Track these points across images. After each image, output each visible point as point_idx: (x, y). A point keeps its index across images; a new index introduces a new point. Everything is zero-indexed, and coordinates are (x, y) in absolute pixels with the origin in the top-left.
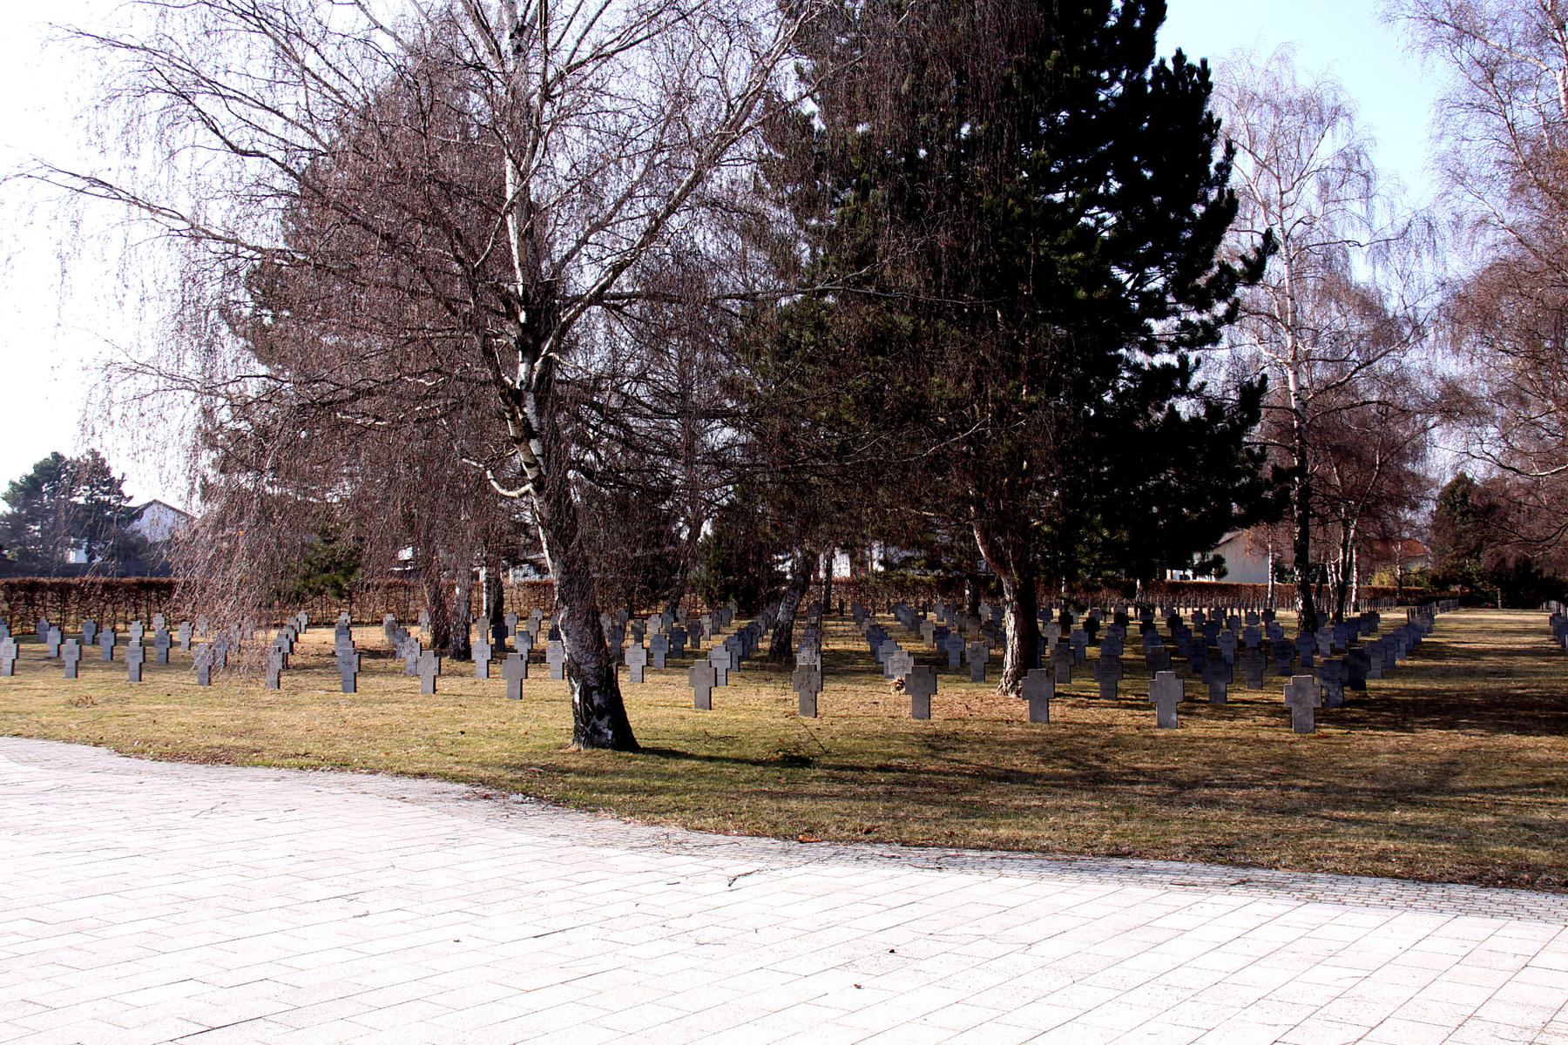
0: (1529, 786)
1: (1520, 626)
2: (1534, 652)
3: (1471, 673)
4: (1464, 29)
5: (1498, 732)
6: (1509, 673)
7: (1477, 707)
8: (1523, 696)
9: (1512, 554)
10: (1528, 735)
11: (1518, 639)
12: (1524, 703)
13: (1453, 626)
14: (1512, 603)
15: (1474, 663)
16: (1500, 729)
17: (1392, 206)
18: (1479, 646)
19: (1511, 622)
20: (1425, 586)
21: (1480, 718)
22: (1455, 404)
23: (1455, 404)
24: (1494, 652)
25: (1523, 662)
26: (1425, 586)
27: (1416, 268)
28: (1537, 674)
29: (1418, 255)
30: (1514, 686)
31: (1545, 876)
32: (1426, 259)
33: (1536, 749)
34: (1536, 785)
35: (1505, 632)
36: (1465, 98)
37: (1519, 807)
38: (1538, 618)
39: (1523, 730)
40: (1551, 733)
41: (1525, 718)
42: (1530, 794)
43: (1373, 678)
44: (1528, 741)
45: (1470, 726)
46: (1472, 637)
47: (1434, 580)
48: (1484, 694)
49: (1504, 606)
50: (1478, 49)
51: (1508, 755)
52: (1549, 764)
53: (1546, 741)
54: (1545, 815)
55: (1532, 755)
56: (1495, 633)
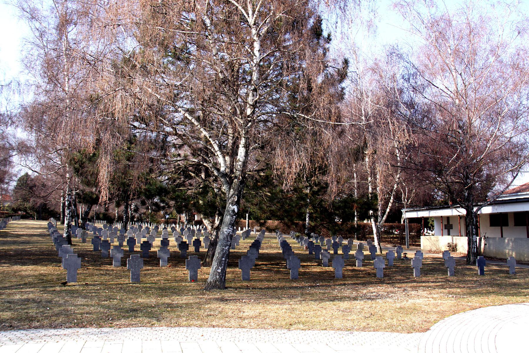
0: (17, 285)
1: (39, 226)
2: (40, 235)
3: (14, 243)
4: (33, 16)
5: (14, 265)
6: (28, 243)
7: (11, 255)
8: (29, 251)
9: (40, 201)
10: (25, 265)
11: (36, 231)
12: (29, 253)
13: (15, 225)
14: (40, 218)
15: (17, 239)
16: (16, 263)
17: (5, 74)
18: (21, 233)
19: (36, 225)
20: (10, 212)
21: (10, 260)
22: (23, 149)
23: (23, 149)
24: (26, 235)
25: (35, 238)
26: (10, 212)
27: (12, 98)
28: (38, 243)
29: (14, 93)
30: (28, 247)
31: (3, 324)
32: (17, 95)
33: (26, 271)
34: (20, 285)
35: (32, 228)
36: (32, 40)
37: (9, 295)
38: (45, 223)
39: (24, 264)
40: (34, 264)
41: (26, 259)
42: (16, 289)
43: (460, 217)
44: (24, 268)
45: (5, 263)
46: (20, 230)
47: (13, 209)
48: (16, 251)
49: (37, 219)
50: (37, 25)
51: (15, 274)
52: (29, 276)
53: (31, 267)
54: (18, 297)
55: (23, 273)
56: (29, 228)
